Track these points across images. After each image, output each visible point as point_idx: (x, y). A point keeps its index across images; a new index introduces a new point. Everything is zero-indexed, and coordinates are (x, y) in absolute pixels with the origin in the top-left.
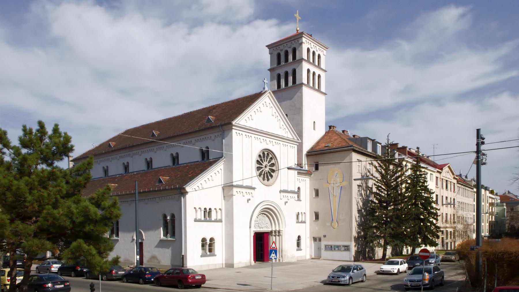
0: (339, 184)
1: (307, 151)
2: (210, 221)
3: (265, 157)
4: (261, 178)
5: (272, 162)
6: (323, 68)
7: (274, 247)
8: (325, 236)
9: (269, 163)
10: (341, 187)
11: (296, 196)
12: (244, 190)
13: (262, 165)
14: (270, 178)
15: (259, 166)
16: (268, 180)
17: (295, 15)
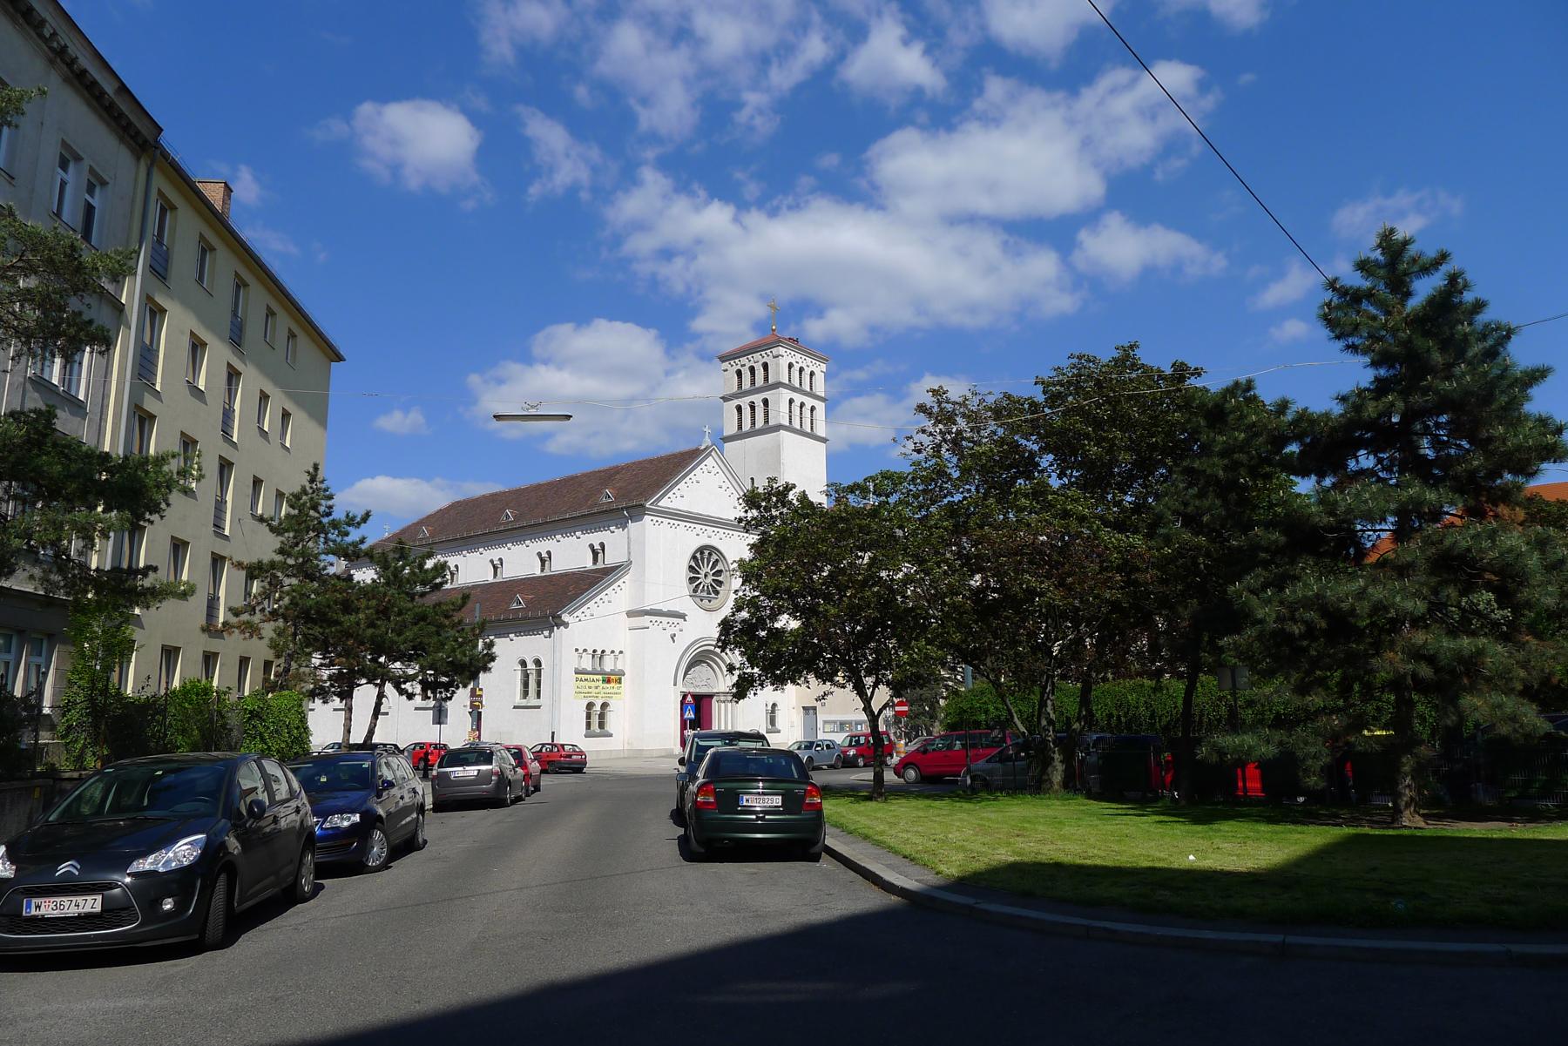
3: (711, 563)
9: (711, 570)
12: (665, 620)
13: (699, 573)
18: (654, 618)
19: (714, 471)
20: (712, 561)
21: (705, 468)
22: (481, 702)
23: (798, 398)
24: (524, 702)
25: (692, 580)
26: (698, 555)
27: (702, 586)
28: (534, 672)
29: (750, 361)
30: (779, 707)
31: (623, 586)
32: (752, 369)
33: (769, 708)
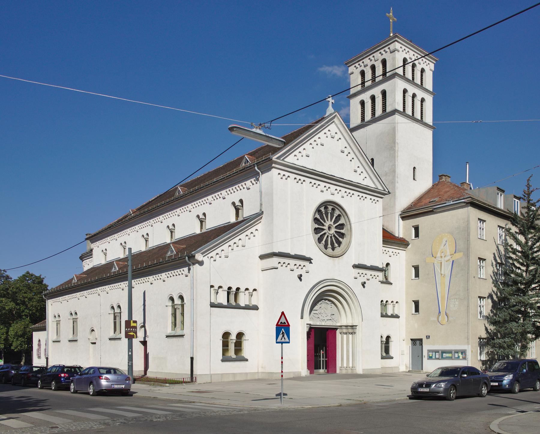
0: (449, 257)
1: (402, 209)
2: (238, 307)
3: (329, 214)
4: (322, 245)
5: (340, 222)
6: (429, 89)
7: (284, 323)
8: (428, 337)
9: (335, 223)
10: (453, 261)
11: (381, 275)
12: (292, 262)
13: (323, 225)
14: (336, 245)
15: (317, 226)
16: (333, 249)
17: (387, 14)
18: (282, 260)
19: (337, 137)
20: (335, 215)
21: (328, 133)
22: (136, 333)
23: (411, 90)
24: (173, 333)
25: (317, 231)
26: (322, 209)
27: (329, 238)
28: (180, 307)
29: (371, 60)
30: (392, 339)
31: (256, 233)
32: (373, 68)
33: (384, 339)
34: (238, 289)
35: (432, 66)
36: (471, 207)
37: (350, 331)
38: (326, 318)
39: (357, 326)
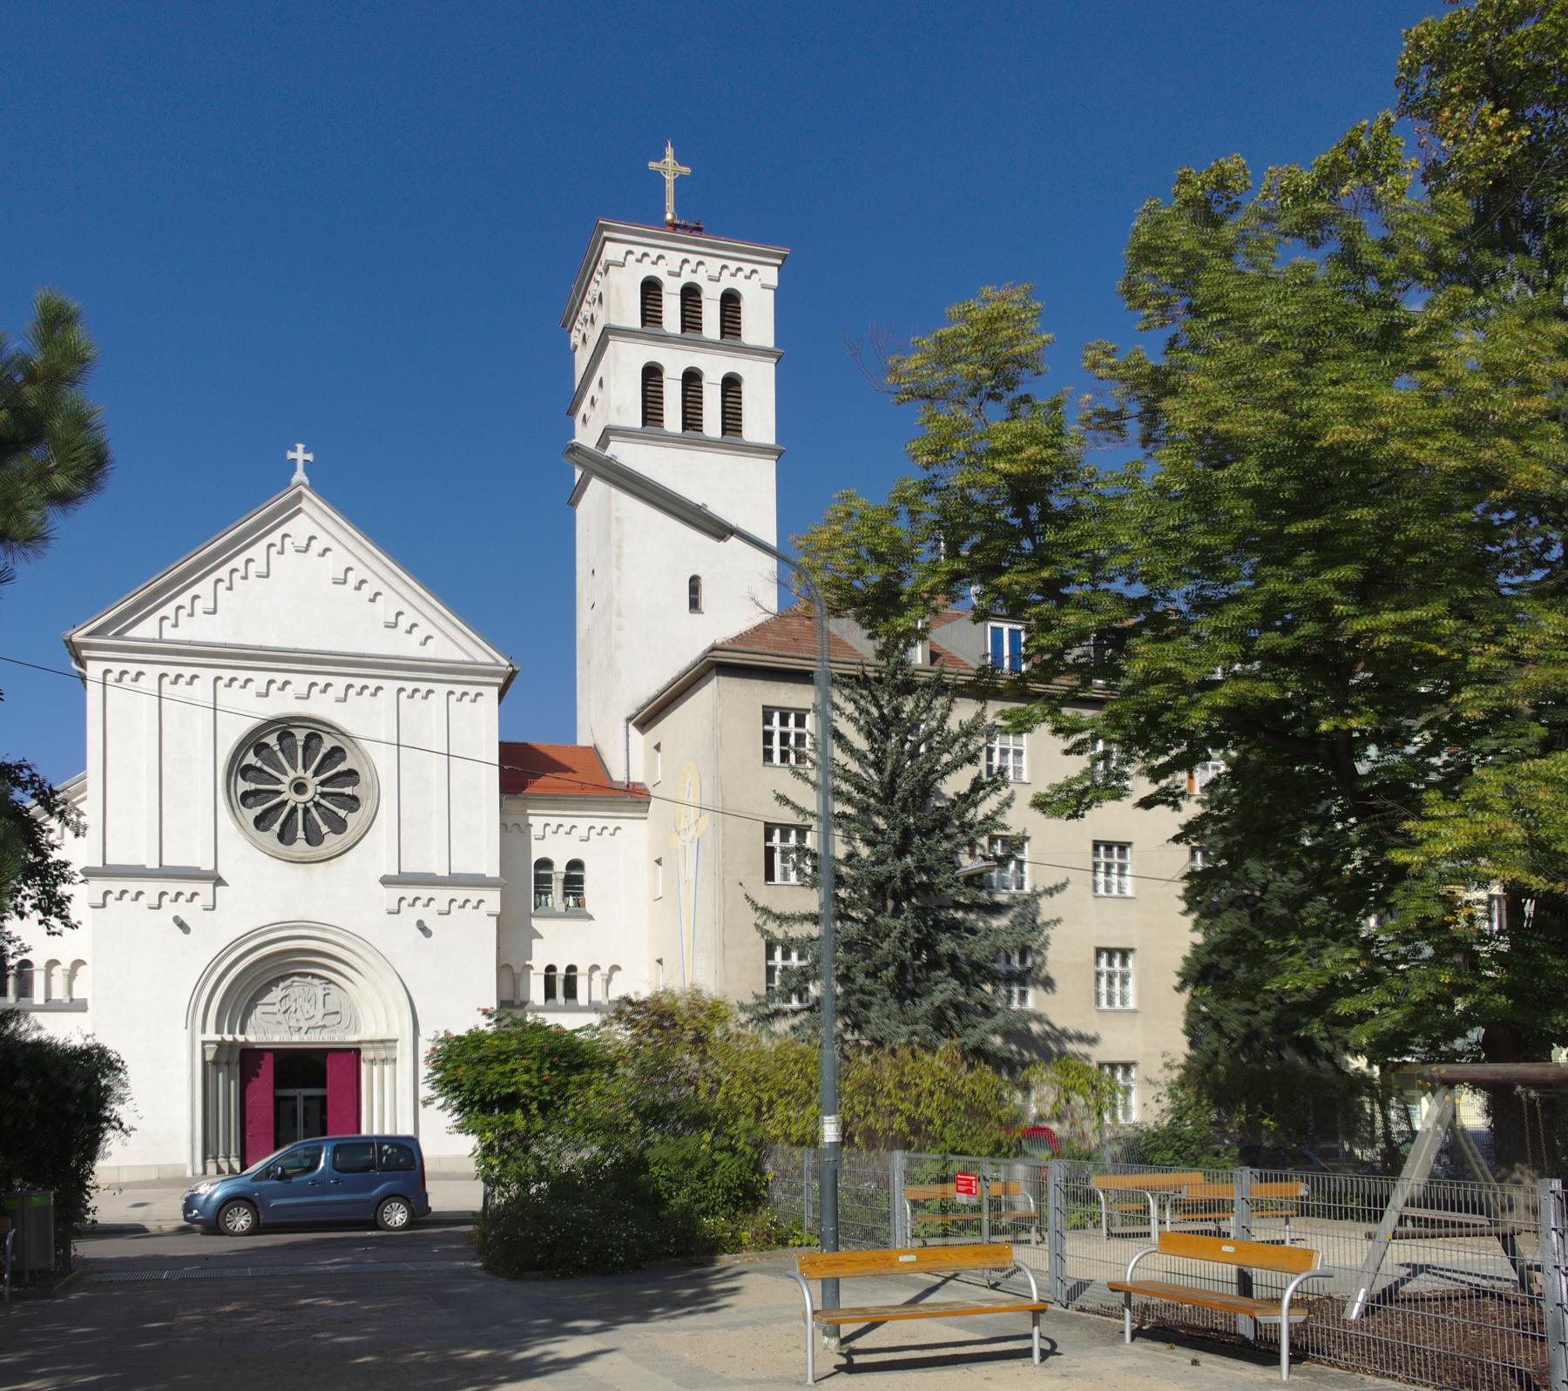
12: (151, 888)
34: (572, 968)
35: (770, 275)
36: (721, 678)
37: (383, 1054)
38: (305, 1025)
39: (396, 1041)
